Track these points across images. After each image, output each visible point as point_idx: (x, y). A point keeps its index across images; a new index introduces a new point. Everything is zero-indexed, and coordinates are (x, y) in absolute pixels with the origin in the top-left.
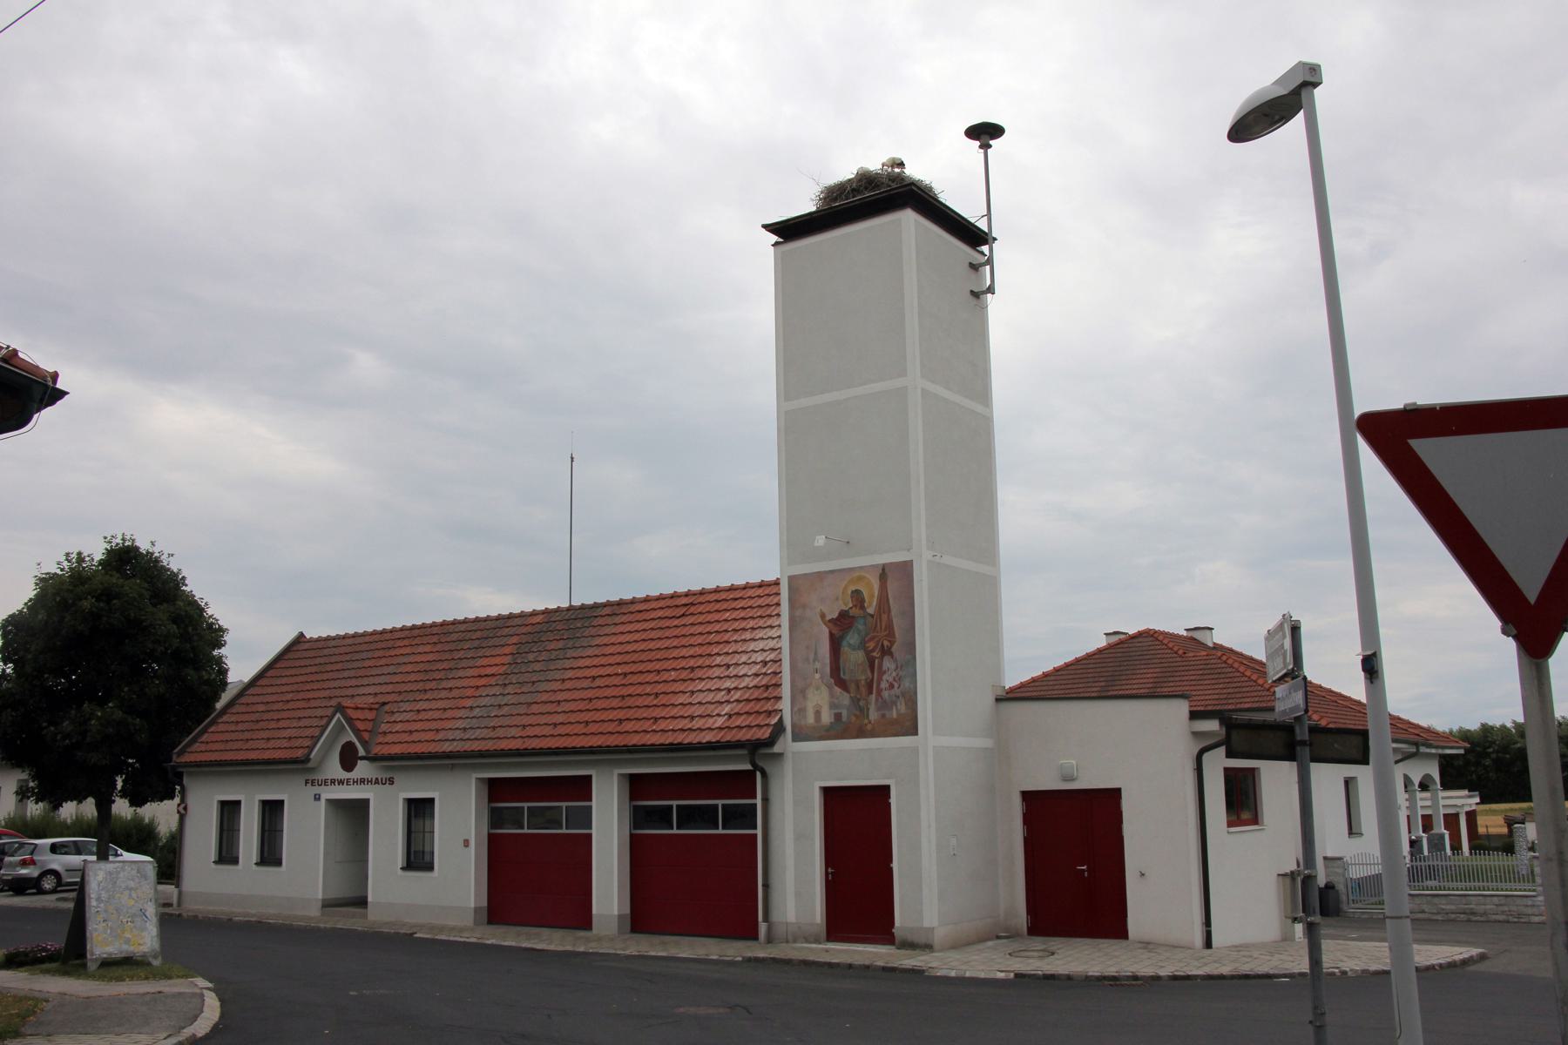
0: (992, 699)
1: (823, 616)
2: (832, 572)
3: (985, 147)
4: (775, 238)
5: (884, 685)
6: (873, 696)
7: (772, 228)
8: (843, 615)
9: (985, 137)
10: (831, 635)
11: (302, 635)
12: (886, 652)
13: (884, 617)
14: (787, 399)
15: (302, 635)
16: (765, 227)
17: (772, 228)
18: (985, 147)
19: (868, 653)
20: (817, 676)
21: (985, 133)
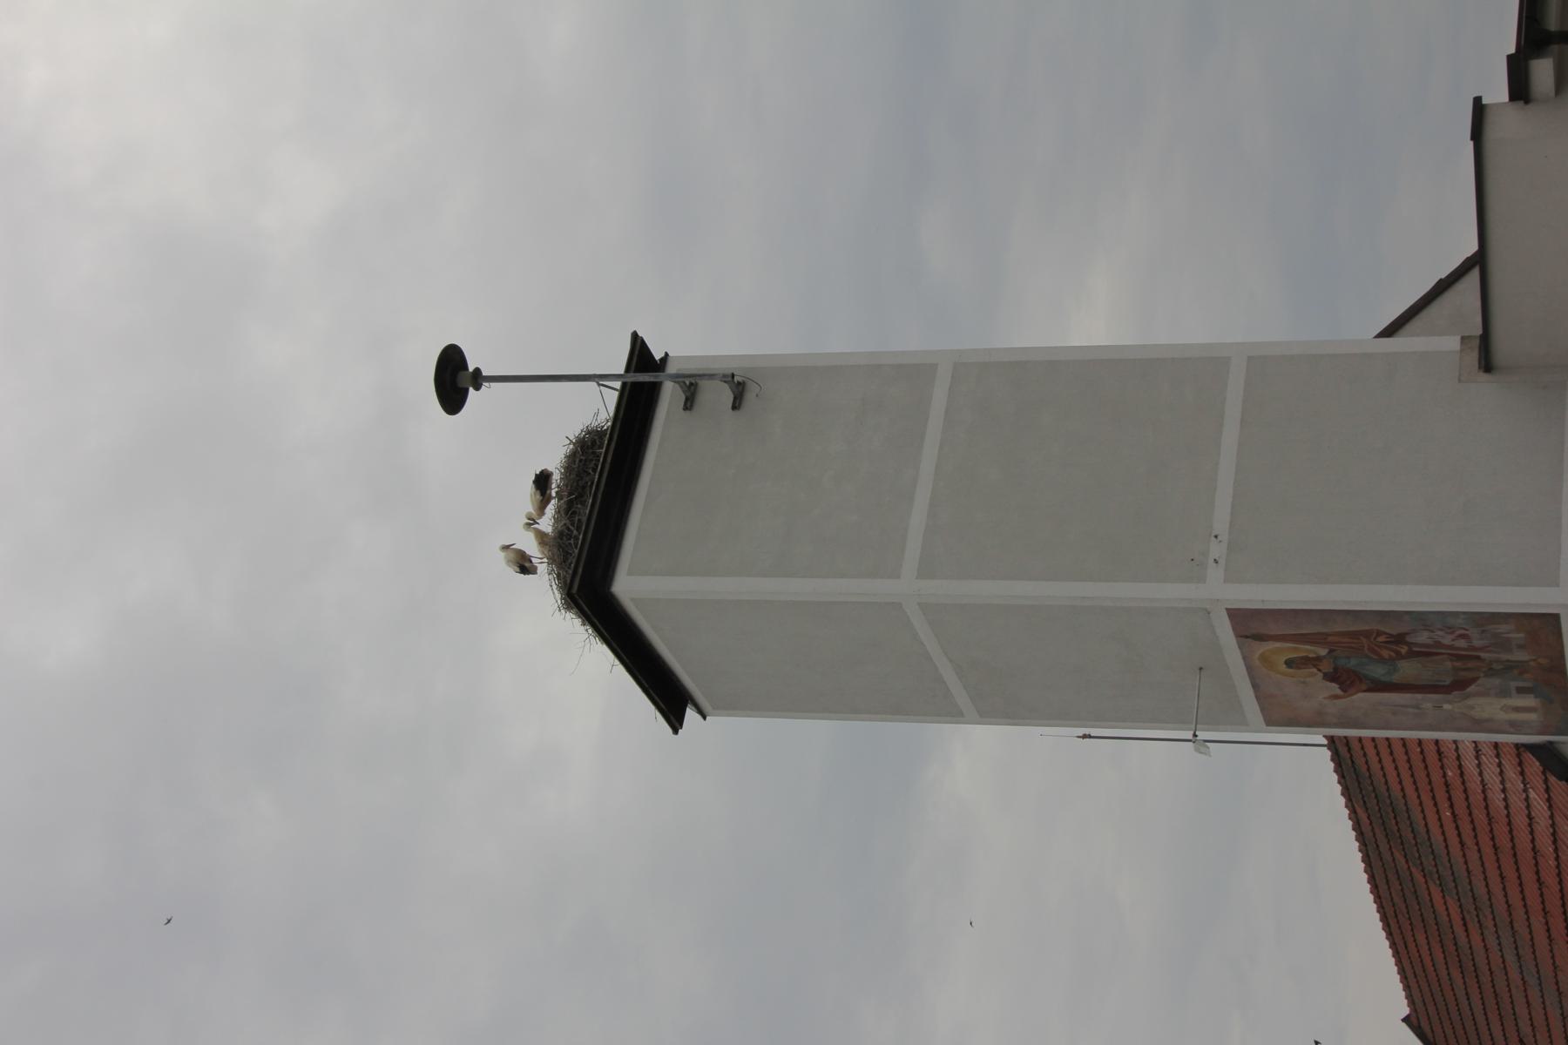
0: (1484, 377)
1: (1336, 697)
2: (1255, 686)
3: (478, 379)
4: (690, 714)
5: (1462, 643)
6: (1482, 655)
7: (676, 722)
8: (1331, 677)
9: (463, 380)
10: (1369, 690)
11: (1406, 1020)
12: (1399, 639)
13: (1330, 639)
14: (961, 714)
15: (1406, 1020)
16: (635, 336)
17: (676, 722)
18: (478, 379)
19: (1400, 656)
20: (1447, 706)
21: (454, 379)
